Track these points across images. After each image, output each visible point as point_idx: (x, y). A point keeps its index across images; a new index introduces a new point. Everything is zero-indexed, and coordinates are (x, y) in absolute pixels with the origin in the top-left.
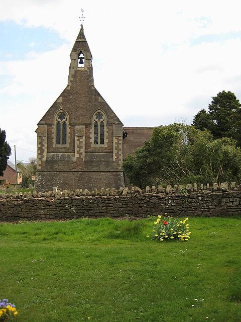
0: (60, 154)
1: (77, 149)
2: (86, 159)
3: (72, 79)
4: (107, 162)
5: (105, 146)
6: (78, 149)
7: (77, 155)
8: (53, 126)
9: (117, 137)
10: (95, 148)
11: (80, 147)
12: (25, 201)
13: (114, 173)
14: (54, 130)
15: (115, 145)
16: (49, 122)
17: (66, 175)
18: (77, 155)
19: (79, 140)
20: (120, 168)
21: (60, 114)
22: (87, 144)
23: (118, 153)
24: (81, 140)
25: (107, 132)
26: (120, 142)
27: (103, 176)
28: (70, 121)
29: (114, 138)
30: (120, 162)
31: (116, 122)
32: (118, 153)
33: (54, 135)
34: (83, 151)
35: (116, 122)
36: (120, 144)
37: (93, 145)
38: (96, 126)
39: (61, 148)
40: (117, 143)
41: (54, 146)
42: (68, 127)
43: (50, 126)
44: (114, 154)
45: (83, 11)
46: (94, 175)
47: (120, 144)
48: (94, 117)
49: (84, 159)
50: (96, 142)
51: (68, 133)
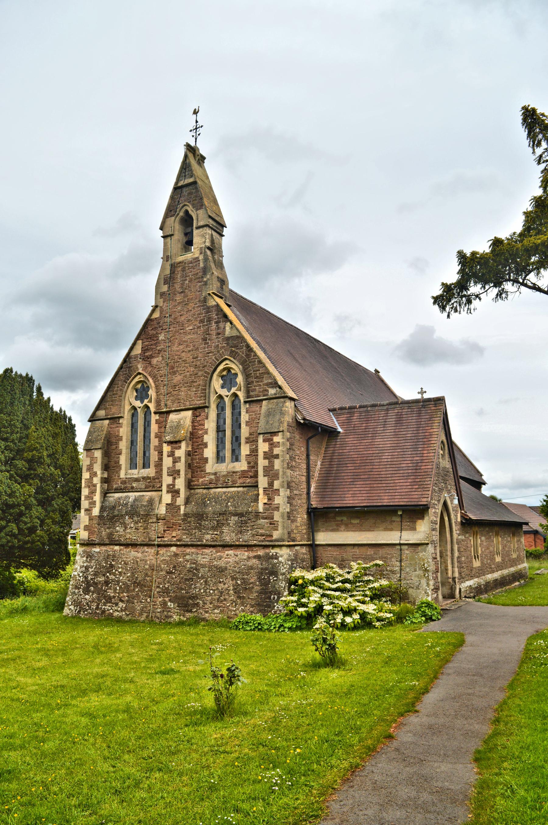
0: (132, 496)
1: (167, 480)
2: (187, 509)
3: (165, 288)
4: (241, 515)
5: (145, 472)
6: (266, 463)
7: (167, 498)
8: (121, 421)
9: (268, 436)
10: (215, 474)
11: (174, 473)
12: (110, 602)
13: (261, 552)
14: (124, 431)
15: (262, 463)
16: (114, 411)
17: (139, 555)
18: (167, 498)
19: (171, 454)
20: (276, 535)
21: (139, 386)
22: (195, 464)
23: (271, 484)
24: (178, 453)
25: (247, 423)
26: (276, 451)
27: (230, 558)
28: (158, 403)
29: (261, 439)
30: (277, 516)
31: (272, 391)
32: (271, 484)
33: (123, 445)
34: (180, 484)
35: (272, 391)
36: (277, 457)
37: (211, 467)
38: (221, 408)
39: (137, 480)
40: (270, 456)
41: (122, 475)
42: (154, 418)
43: (115, 420)
44: (261, 491)
45: (196, 112)
46: (204, 557)
47: (277, 457)
48: (217, 383)
49: (182, 508)
50: (220, 458)
51: (153, 435)
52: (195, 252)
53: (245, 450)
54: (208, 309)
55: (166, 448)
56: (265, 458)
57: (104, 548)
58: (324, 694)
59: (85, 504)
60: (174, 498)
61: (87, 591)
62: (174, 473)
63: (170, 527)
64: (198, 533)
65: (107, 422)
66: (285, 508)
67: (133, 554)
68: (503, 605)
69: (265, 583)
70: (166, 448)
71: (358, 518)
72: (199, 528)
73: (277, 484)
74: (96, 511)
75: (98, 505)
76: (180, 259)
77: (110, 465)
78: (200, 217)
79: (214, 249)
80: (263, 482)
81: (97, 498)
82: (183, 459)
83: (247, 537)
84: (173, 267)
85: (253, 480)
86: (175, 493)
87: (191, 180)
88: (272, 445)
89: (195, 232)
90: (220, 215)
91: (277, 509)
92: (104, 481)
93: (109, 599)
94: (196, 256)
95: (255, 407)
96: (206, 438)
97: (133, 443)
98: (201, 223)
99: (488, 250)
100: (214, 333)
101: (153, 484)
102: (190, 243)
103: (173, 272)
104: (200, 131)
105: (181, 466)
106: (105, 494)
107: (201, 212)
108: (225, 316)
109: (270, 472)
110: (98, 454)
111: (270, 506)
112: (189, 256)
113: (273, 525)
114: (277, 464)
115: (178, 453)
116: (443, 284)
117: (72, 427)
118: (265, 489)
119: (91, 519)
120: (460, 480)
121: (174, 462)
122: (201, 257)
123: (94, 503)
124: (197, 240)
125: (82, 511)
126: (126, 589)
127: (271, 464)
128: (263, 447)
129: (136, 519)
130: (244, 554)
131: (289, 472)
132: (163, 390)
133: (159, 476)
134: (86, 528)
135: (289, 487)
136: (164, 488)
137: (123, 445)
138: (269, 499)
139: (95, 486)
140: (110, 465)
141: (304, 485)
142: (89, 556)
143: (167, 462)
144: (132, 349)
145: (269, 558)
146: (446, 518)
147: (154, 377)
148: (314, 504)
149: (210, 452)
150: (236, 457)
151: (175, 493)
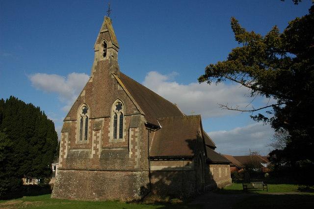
1: (94, 145)
7: (93, 152)
11: (97, 142)
15: (131, 139)
16: (73, 118)
18: (93, 152)
19: (95, 135)
23: (134, 147)
24: (98, 135)
25: (125, 124)
26: (136, 135)
27: (118, 175)
30: (136, 160)
33: (77, 131)
35: (135, 112)
36: (136, 137)
42: (89, 121)
46: (108, 174)
47: (136, 137)
50: (115, 136)
52: (107, 57)
53: (124, 134)
55: (94, 132)
56: (132, 137)
57: (68, 171)
59: (61, 153)
60: (96, 152)
61: (60, 188)
62: (97, 142)
63: (94, 163)
64: (105, 165)
65: (71, 121)
66: (139, 157)
67: (81, 173)
69: (131, 185)
70: (94, 132)
72: (106, 164)
73: (136, 147)
74: (65, 157)
75: (66, 154)
76: (101, 60)
77: (72, 139)
80: (131, 147)
81: (66, 151)
82: (100, 137)
83: (125, 167)
86: (96, 150)
87: (107, 30)
88: (135, 132)
89: (107, 50)
91: (136, 157)
92: (69, 145)
93: (69, 192)
94: (108, 59)
95: (129, 117)
96: (109, 129)
97: (81, 130)
98: (110, 47)
100: (113, 89)
101: (88, 146)
103: (98, 64)
105: (99, 140)
106: (69, 150)
107: (110, 42)
108: (118, 83)
109: (133, 142)
110: (67, 134)
111: (133, 155)
113: (135, 163)
114: (137, 140)
115: (98, 135)
116: (187, 141)
117: (57, 145)
118: (132, 149)
119: (63, 159)
120: (206, 147)
121: (97, 138)
123: (65, 153)
124: (108, 53)
125: (60, 156)
126: (77, 187)
127: (134, 139)
128: (131, 133)
129: (81, 159)
130: (124, 174)
131: (141, 143)
132: (93, 110)
133: (90, 144)
134: (61, 163)
135: (141, 148)
136: (93, 147)
137: (77, 131)
138: (133, 153)
139: (65, 146)
140: (72, 139)
141: (147, 148)
142: (62, 174)
143: (94, 138)
144: (81, 93)
145: (132, 175)
146: (200, 161)
148: (151, 156)
149: (111, 134)
150: (121, 137)
151: (96, 150)
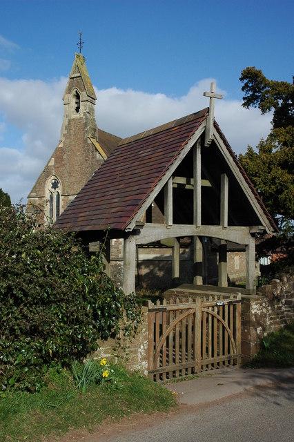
42: (61, 198)
52: (81, 114)
54: (88, 145)
58: (111, 290)
68: (155, 346)
71: (166, 257)
76: (73, 117)
78: (83, 96)
79: (91, 112)
84: (69, 121)
85: (171, 313)
87: (79, 75)
90: (94, 94)
98: (85, 99)
99: (201, 261)
102: (77, 109)
103: (69, 124)
104: (83, 45)
112: (77, 116)
122: (84, 117)
124: (82, 108)
147: (61, 177)
